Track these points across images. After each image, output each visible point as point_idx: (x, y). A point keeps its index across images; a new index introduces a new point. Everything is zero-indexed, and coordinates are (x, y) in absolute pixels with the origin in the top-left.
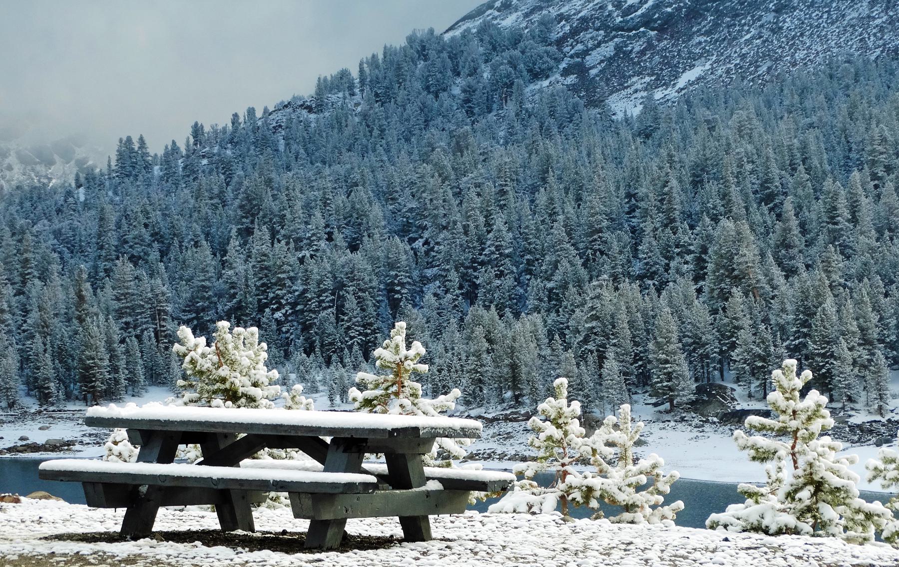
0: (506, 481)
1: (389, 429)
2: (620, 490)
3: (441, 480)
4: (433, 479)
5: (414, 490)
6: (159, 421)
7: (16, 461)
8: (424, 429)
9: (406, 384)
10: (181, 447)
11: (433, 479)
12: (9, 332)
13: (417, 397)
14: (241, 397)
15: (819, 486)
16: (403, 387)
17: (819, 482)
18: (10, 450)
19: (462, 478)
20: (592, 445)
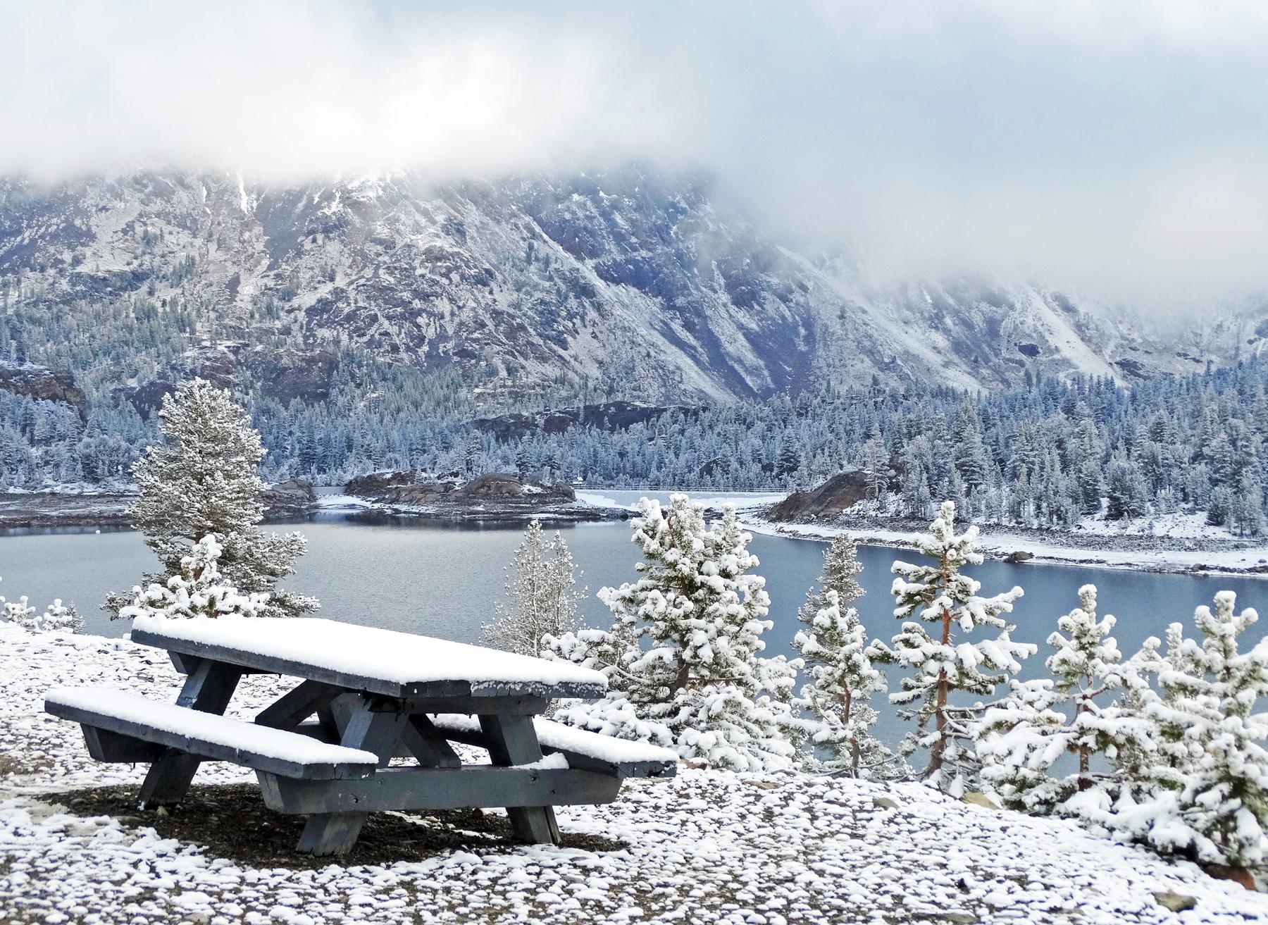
0: (657, 763)
1: (403, 682)
2: (1149, 735)
3: (569, 755)
4: (559, 751)
5: (515, 767)
6: (192, 642)
7: (1254, 580)
8: (479, 683)
9: (953, 578)
10: (244, 676)
11: (559, 751)
12: (1256, 472)
13: (968, 595)
14: (698, 588)
15: (1240, 787)
16: (949, 581)
17: (1239, 779)
18: (1250, 570)
19: (589, 754)
20: (1122, 674)
